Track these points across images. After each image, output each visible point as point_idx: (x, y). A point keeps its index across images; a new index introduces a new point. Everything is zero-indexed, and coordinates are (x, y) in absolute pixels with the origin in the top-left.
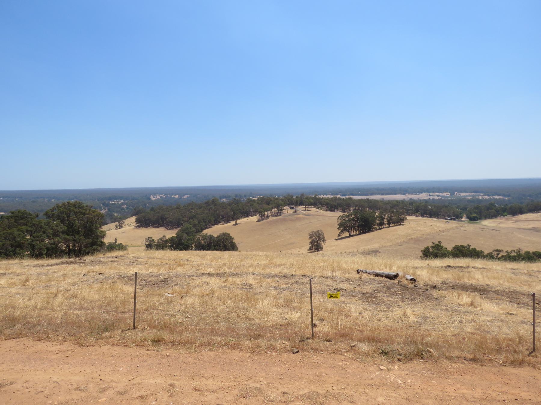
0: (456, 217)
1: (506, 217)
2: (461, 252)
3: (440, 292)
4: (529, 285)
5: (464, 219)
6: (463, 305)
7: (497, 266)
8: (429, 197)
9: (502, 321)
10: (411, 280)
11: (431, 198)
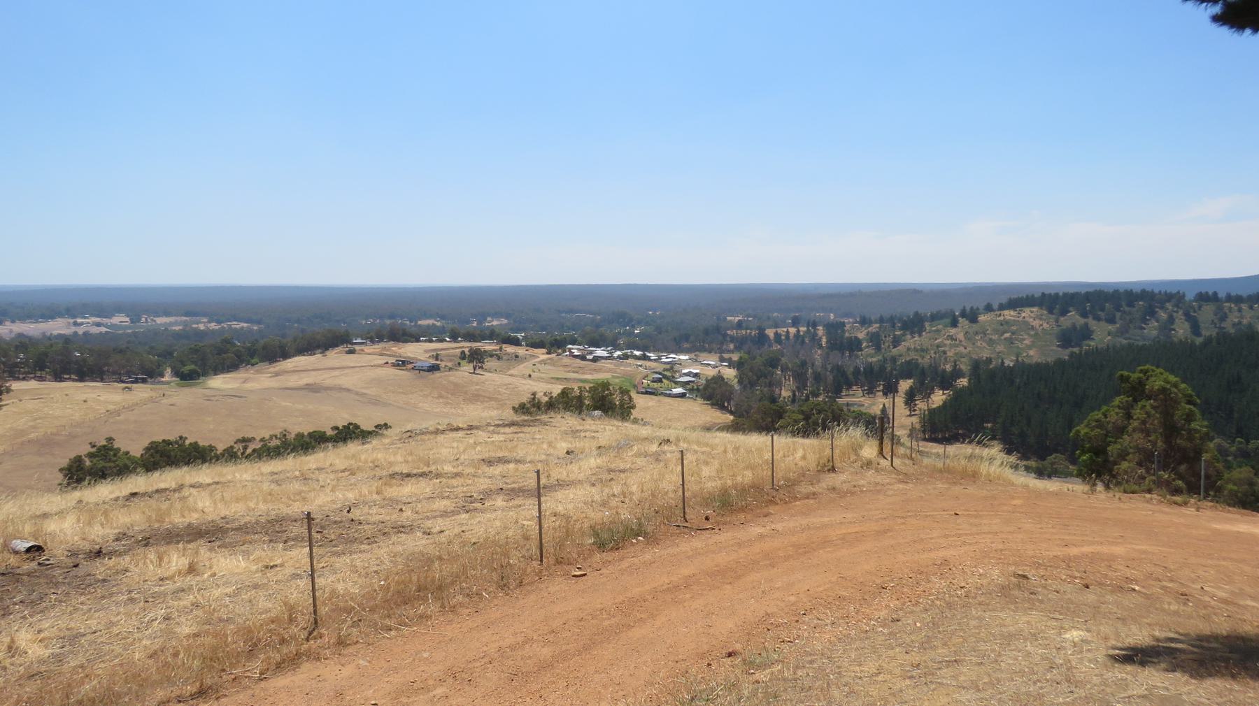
0: (149, 374)
1: (256, 367)
2: (165, 455)
3: (111, 563)
5: (167, 378)
6: (171, 578)
7: (243, 474)
8: (73, 329)
9: (256, 586)
10: (29, 550)
11: (81, 330)
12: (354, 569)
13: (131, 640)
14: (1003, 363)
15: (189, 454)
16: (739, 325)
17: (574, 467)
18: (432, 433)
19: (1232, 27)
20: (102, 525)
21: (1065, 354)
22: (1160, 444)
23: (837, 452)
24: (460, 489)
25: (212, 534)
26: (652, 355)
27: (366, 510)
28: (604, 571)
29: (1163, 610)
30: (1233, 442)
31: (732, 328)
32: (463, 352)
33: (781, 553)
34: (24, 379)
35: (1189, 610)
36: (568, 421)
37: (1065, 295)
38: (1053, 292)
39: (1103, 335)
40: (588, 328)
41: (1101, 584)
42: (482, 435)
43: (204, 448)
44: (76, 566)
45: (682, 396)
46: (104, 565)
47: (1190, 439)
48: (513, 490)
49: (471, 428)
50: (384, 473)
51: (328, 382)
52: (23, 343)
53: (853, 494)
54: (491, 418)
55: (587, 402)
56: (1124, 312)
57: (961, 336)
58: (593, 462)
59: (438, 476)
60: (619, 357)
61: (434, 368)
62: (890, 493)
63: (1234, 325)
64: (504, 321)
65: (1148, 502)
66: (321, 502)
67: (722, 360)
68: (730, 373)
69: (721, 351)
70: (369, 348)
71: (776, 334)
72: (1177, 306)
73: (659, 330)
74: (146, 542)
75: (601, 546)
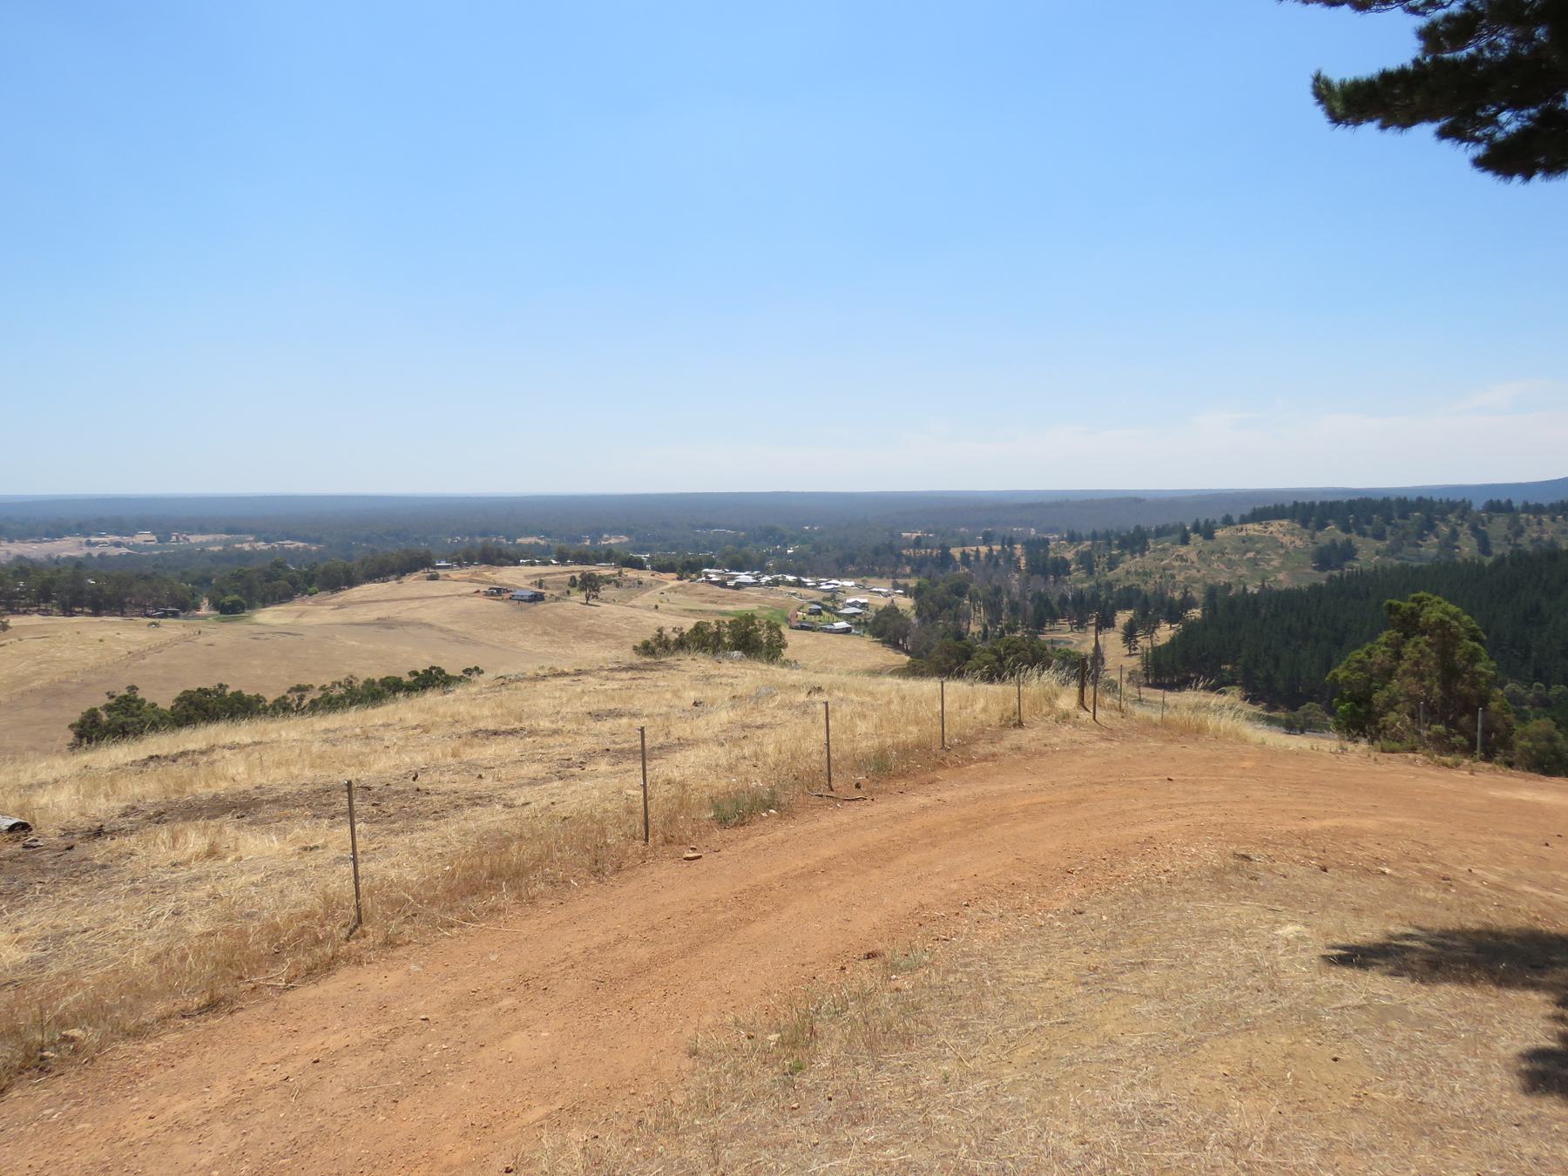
0: (181, 606)
1: (315, 597)
2: (201, 708)
3: (114, 844)
4: (361, 764)
5: (204, 611)
6: (187, 863)
7: (289, 731)
8: (86, 550)
9: (290, 873)
10: (12, 829)
11: (95, 552)
12: (413, 851)
13: (129, 941)
14: (1245, 589)
15: (231, 707)
16: (918, 543)
17: (701, 722)
18: (531, 679)
19: (1497, 173)
20: (107, 796)
21: (1322, 578)
22: (1436, 690)
23: (1026, 703)
24: (557, 750)
25: (244, 807)
26: (808, 581)
27: (436, 777)
28: (724, 852)
29: (1415, 898)
30: (1530, 686)
31: (908, 547)
32: (573, 578)
33: (946, 829)
34: (25, 613)
35: (1449, 898)
36: (699, 664)
37: (1323, 504)
38: (1307, 501)
39: (1369, 554)
40: (729, 548)
41: (1342, 866)
42: (591, 682)
43: (250, 699)
44: (70, 848)
45: (847, 631)
46: (104, 847)
47: (1474, 684)
48: (622, 751)
49: (579, 672)
50: (465, 730)
51: (405, 616)
52: (23, 568)
53: (1042, 754)
54: (605, 659)
55: (726, 640)
56: (1396, 526)
57: (1193, 556)
58: (724, 716)
59: (532, 733)
60: (768, 584)
61: (537, 598)
62: (1090, 753)
63: (1532, 541)
64: (625, 539)
65: (1410, 763)
66: (382, 766)
67: (896, 586)
68: (905, 603)
69: (895, 576)
70: (456, 574)
71: (963, 553)
72: (1462, 518)
73: (818, 549)
74: (159, 817)
75: (723, 821)
